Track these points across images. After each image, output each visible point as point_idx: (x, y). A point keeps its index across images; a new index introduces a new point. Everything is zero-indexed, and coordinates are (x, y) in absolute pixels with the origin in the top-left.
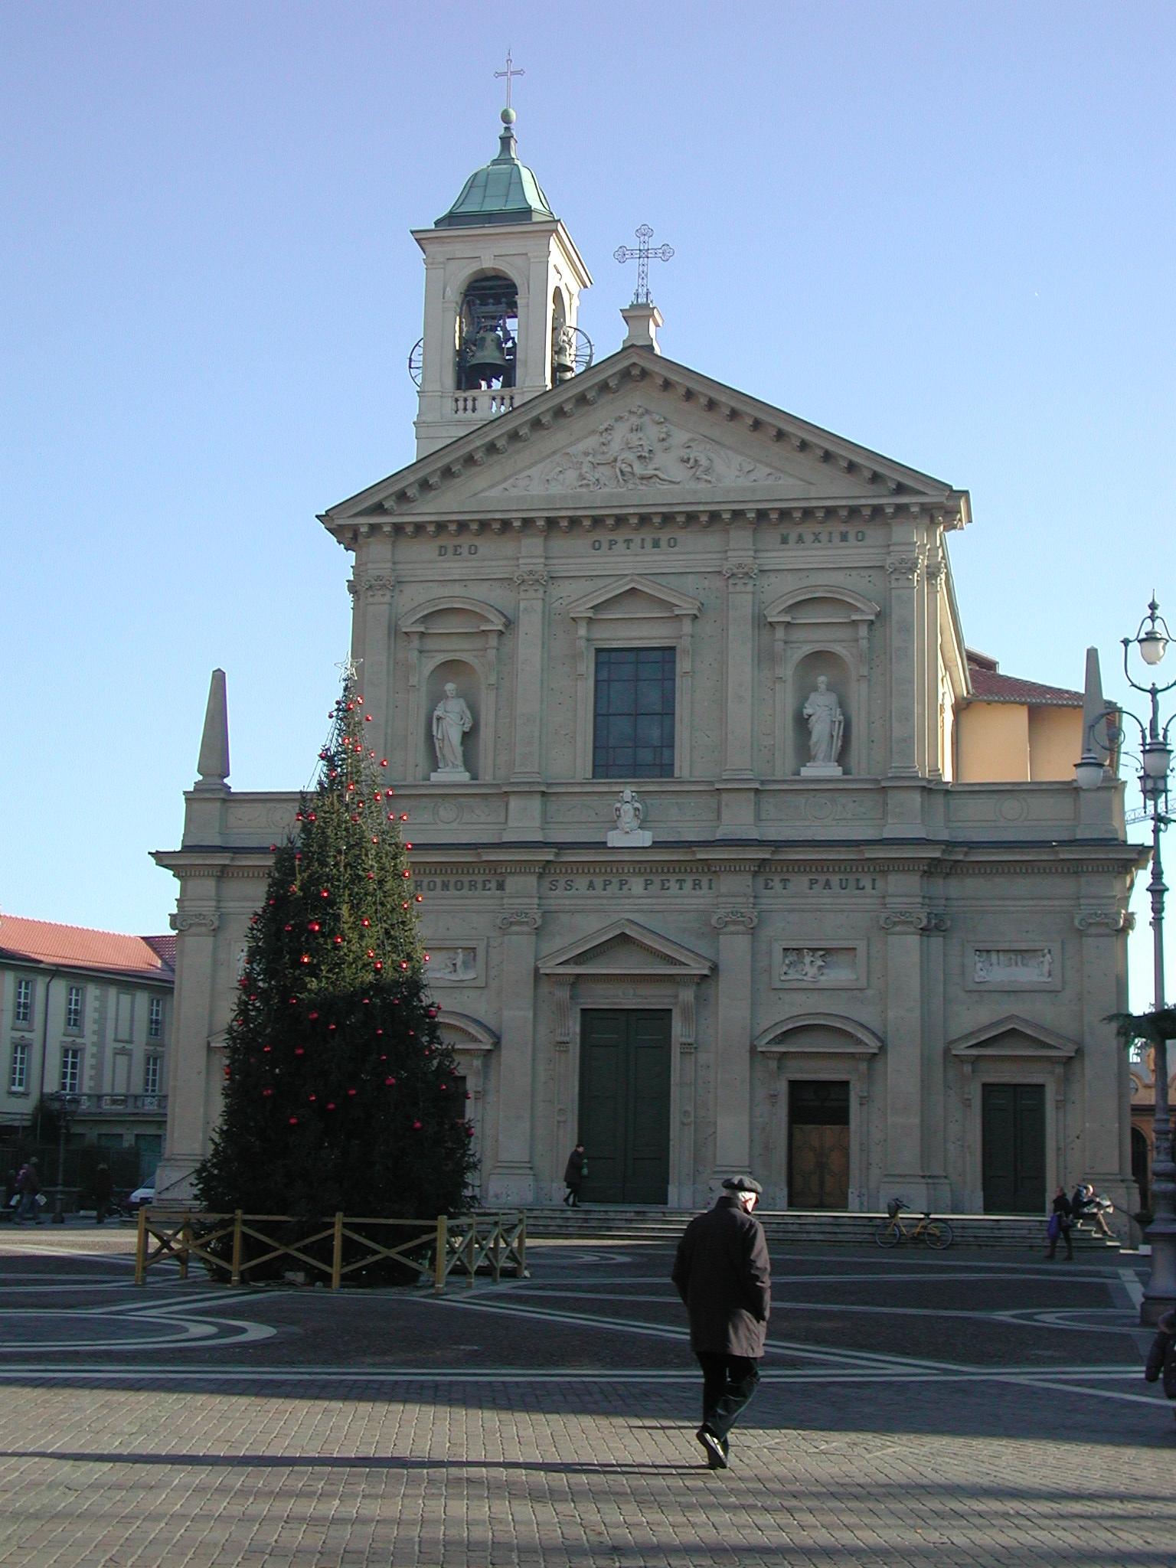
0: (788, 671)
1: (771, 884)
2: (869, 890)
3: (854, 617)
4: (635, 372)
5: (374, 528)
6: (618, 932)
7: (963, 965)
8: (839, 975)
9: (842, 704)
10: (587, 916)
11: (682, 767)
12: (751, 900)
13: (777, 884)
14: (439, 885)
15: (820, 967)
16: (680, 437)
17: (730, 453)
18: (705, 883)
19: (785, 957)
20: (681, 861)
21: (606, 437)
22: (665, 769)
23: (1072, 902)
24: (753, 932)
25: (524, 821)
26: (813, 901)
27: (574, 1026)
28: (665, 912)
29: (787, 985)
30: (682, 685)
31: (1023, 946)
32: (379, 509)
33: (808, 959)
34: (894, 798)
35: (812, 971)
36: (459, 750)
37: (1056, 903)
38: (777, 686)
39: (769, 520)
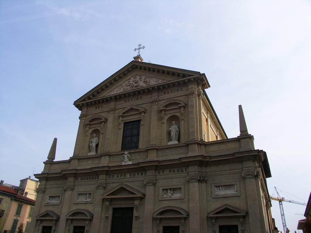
0: (165, 121)
1: (160, 172)
2: (185, 171)
3: (179, 106)
4: (134, 66)
5: (83, 104)
6: (120, 187)
7: (212, 191)
8: (177, 195)
9: (179, 128)
10: (114, 183)
11: (141, 146)
12: (154, 176)
13: (161, 172)
14: (86, 178)
15: (172, 193)
16: (143, 77)
17: (153, 79)
18: (144, 173)
19: (163, 191)
20: (138, 169)
21: (129, 81)
22: (137, 147)
23: (242, 170)
24: (154, 184)
25: (105, 162)
26: (171, 176)
27: (111, 213)
28: (133, 183)
29: (163, 199)
30: (141, 127)
31: (228, 184)
32: (84, 100)
33: (169, 192)
34: (190, 147)
35: (170, 195)
36: (95, 148)
37: (237, 170)
38: (163, 125)
39: (160, 89)
